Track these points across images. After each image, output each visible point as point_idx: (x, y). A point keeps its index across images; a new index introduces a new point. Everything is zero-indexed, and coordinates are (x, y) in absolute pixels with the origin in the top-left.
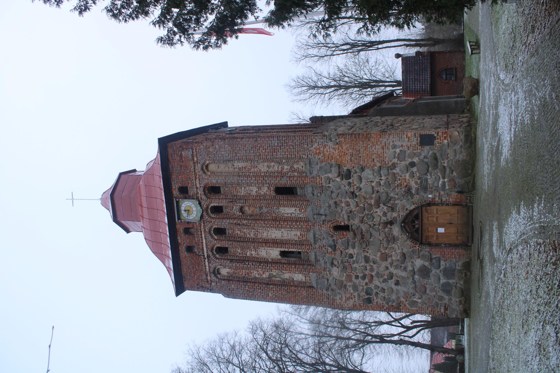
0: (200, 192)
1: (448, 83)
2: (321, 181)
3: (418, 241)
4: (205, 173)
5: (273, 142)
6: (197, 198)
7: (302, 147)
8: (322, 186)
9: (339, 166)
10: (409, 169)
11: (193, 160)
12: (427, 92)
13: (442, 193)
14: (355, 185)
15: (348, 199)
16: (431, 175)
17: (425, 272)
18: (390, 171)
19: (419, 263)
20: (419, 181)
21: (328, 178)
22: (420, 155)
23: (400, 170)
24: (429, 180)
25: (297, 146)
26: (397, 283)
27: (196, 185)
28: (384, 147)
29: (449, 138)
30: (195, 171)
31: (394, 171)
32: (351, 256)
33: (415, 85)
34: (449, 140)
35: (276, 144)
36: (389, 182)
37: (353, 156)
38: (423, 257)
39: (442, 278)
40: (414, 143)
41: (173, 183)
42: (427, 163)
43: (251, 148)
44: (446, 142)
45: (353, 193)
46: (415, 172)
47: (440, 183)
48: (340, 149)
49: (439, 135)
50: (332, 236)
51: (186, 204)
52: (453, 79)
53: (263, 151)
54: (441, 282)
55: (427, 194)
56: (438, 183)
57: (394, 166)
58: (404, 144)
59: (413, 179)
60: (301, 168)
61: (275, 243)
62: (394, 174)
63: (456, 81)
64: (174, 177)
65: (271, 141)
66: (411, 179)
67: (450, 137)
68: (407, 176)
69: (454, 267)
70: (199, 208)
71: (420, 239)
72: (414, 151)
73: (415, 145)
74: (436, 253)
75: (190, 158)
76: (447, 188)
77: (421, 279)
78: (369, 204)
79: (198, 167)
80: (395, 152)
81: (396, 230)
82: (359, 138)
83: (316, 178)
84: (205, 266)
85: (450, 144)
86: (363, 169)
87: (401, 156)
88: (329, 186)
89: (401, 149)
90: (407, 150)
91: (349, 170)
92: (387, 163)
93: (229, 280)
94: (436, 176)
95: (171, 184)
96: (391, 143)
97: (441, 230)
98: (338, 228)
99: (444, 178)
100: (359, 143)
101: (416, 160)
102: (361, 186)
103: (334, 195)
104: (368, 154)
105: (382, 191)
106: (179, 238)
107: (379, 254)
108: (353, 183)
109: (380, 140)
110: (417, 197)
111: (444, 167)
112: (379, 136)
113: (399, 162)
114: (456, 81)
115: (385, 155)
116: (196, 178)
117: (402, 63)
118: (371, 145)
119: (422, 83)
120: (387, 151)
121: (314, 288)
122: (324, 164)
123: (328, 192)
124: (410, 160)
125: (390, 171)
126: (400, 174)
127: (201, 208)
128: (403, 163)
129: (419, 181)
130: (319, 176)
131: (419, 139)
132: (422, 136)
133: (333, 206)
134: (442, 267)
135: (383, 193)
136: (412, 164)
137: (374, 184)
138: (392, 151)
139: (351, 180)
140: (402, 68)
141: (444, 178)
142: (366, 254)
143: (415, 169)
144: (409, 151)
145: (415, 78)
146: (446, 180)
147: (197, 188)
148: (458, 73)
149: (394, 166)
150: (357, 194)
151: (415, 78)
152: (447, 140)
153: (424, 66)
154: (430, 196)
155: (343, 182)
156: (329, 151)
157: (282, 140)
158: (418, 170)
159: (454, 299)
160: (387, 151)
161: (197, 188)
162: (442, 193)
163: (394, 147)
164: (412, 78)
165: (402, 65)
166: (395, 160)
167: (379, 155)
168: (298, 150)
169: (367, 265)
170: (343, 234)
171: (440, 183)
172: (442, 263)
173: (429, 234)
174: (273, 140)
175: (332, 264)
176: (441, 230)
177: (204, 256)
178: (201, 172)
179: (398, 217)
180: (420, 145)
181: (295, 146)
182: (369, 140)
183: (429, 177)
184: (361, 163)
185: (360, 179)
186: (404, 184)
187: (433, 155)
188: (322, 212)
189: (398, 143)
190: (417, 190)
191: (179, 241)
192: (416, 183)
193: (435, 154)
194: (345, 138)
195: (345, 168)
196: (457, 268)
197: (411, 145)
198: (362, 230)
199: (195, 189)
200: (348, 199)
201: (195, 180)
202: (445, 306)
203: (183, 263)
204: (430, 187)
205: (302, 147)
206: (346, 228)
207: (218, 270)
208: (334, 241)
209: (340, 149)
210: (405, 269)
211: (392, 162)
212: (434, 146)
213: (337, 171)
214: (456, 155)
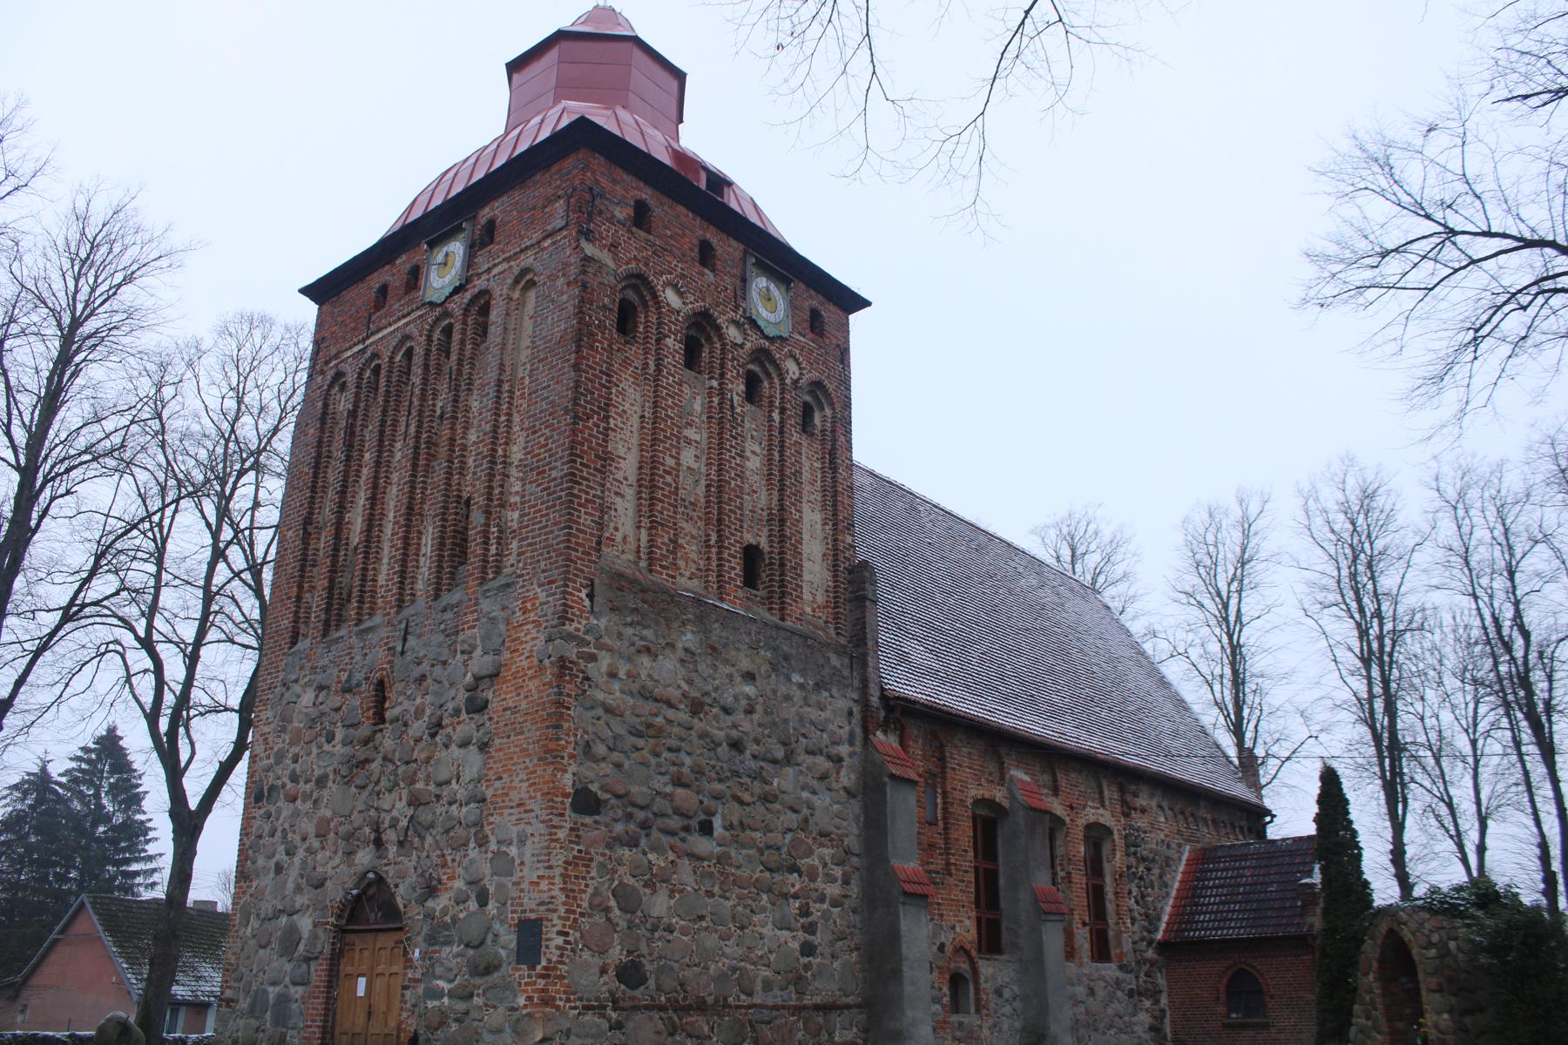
0: (480, 284)
1: (1218, 999)
2: (469, 628)
3: (349, 921)
4: (517, 281)
5: (558, 464)
6: (468, 280)
7: (542, 554)
8: (457, 632)
9: (494, 676)
10: (473, 887)
11: (545, 238)
12: (1183, 930)
13: (421, 989)
14: (454, 730)
15: (428, 712)
16: (458, 955)
17: (290, 940)
18: (473, 830)
19: (305, 923)
20: (448, 919)
21: (474, 647)
22: (502, 922)
23: (472, 861)
24: (448, 949)
25: (545, 540)
26: (279, 869)
27: (495, 265)
28: (522, 809)
29: (529, 1010)
30: (522, 251)
31: (472, 845)
32: (330, 738)
33: (1217, 887)
34: (524, 1012)
35: (554, 474)
36: (453, 828)
37: (512, 713)
38: (314, 937)
39: (277, 989)
40: (526, 900)
41: (505, 198)
42: (482, 943)
43: (552, 402)
44: (521, 1001)
45: (439, 725)
46: (466, 905)
47: (441, 983)
48: (530, 672)
49: (539, 981)
50: (367, 679)
51: (457, 248)
52: (1234, 1015)
53: (542, 439)
54: (271, 989)
55: (423, 945)
56: (440, 978)
57: (482, 842)
58: (526, 870)
59: (452, 902)
60: (509, 563)
61: (373, 521)
62: (466, 844)
63: (1226, 1026)
64: (516, 195)
65: (561, 458)
66: (452, 895)
67: (530, 1015)
68: (459, 884)
69: (291, 1023)
70: (447, 291)
71: (355, 927)
72: (509, 902)
73: (521, 905)
74: (318, 972)
75: (549, 227)
76: (430, 1004)
77: (279, 933)
78: (415, 773)
79: (528, 260)
80: (510, 844)
81: (364, 857)
82: (548, 727)
83: (475, 611)
84: (350, 348)
85: (516, 1015)
86: (484, 747)
87: (503, 864)
88: (456, 651)
89: (517, 861)
90: (515, 879)
91: (486, 706)
92: (491, 819)
93: (323, 420)
94: (455, 972)
95: (500, 195)
96: (529, 830)
97: (362, 984)
98: (381, 686)
99: (451, 995)
100: (537, 729)
101: (492, 907)
102: (454, 747)
103: (438, 669)
104: (512, 758)
105: (438, 811)
106: (404, 257)
107: (329, 813)
108: (459, 723)
109: (539, 794)
110: (418, 914)
111: (471, 996)
112: (546, 790)
113: (490, 855)
114: (1226, 1026)
115: (507, 811)
116: (507, 260)
117: (1301, 838)
118: (530, 765)
119: (1217, 912)
120: (514, 818)
121: (290, 648)
122: (502, 627)
123: (444, 656)
124: (492, 890)
125: (473, 830)
126: (466, 862)
127: (447, 298)
128: (486, 869)
129: (448, 919)
130: (477, 620)
131: (533, 916)
132: (538, 923)
133: (417, 672)
134: (292, 989)
135: (434, 813)
136: (483, 899)
137: (454, 785)
138: (514, 831)
139: (464, 716)
140: (1284, 840)
141: (451, 995)
142: (331, 777)
143: (473, 905)
144: (510, 885)
145: (1239, 885)
146: (446, 1000)
147: (489, 270)
148: (1251, 1033)
149: (482, 842)
150: (438, 739)
151: (1239, 885)
152: (525, 1006)
153: (1269, 913)
154: (417, 954)
155: (463, 691)
156: (528, 637)
157: (562, 490)
158: (474, 913)
159: (241, 1022)
160: (514, 818)
161: (489, 270)
162: (421, 989)
163: (522, 842)
164: (1242, 876)
165: (1294, 839)
166: (493, 846)
167: (507, 794)
168: (535, 544)
169: (313, 783)
170: (369, 709)
171: (441, 983)
172: (300, 989)
173: (357, 953)
174: (563, 464)
175: (321, 688)
176: (362, 984)
177: (368, 337)
178: (516, 271)
179: (385, 861)
180: (520, 921)
181: (546, 534)
182: (540, 759)
183: (455, 949)
184: (497, 741)
185: (464, 744)
186: (444, 874)
187: (496, 962)
188: (412, 641)
189: (529, 848)
190: (430, 916)
191: (398, 261)
192: (445, 912)
193: (497, 967)
194: (550, 684)
195: (490, 696)
196: (290, 1033)
197: (522, 891)
198: (373, 761)
199: (486, 267)
200: (428, 712)
201: (504, 260)
202: (232, 1001)
203: (361, 285)
204: (434, 952)
205: (542, 554)
206: (380, 718)
207: (531, 284)
208: (359, 685)
209: (530, 672)
210: (298, 889)
211: (489, 833)
212: (514, 964)
213: (484, 672)
214: (491, 1032)
